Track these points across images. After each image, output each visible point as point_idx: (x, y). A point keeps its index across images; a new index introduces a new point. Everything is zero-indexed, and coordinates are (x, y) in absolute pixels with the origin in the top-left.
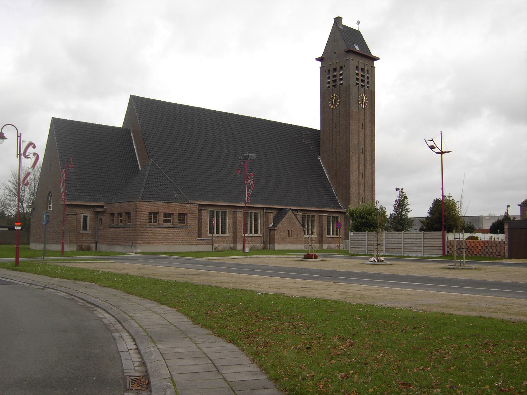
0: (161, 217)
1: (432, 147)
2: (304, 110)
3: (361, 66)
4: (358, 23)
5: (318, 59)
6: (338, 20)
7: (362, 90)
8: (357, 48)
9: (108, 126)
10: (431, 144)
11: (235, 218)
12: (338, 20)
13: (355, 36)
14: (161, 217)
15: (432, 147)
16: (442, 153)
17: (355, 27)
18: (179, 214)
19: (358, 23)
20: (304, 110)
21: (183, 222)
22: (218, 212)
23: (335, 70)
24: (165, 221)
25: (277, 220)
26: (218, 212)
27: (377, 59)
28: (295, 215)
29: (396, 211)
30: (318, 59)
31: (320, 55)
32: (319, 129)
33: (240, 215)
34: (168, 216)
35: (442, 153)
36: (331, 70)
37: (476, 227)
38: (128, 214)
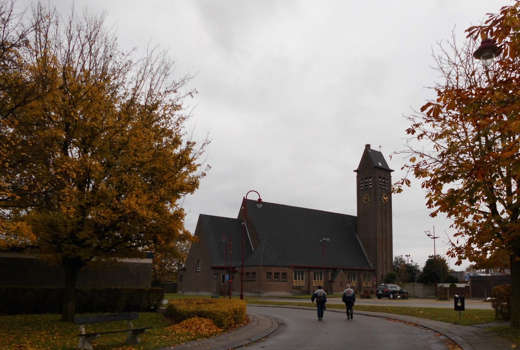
0: (280, 276)
1: (429, 235)
2: (342, 199)
3: (383, 176)
4: (380, 147)
5: (355, 171)
6: (368, 146)
7: (384, 191)
8: (380, 164)
9: (233, 219)
10: (428, 233)
11: (309, 275)
12: (368, 146)
13: (379, 155)
14: (280, 276)
15: (429, 235)
16: (434, 238)
17: (377, 149)
18: (275, 273)
19: (380, 147)
20: (342, 199)
21: (277, 278)
22: (299, 271)
23: (366, 178)
24: (275, 278)
25: (334, 276)
26: (299, 271)
27: (393, 171)
28: (345, 272)
29: (397, 262)
30: (355, 171)
31: (356, 168)
32: (355, 214)
33: (312, 273)
34: (277, 274)
35: (434, 238)
36: (364, 178)
37: (460, 280)
38: (254, 273)
